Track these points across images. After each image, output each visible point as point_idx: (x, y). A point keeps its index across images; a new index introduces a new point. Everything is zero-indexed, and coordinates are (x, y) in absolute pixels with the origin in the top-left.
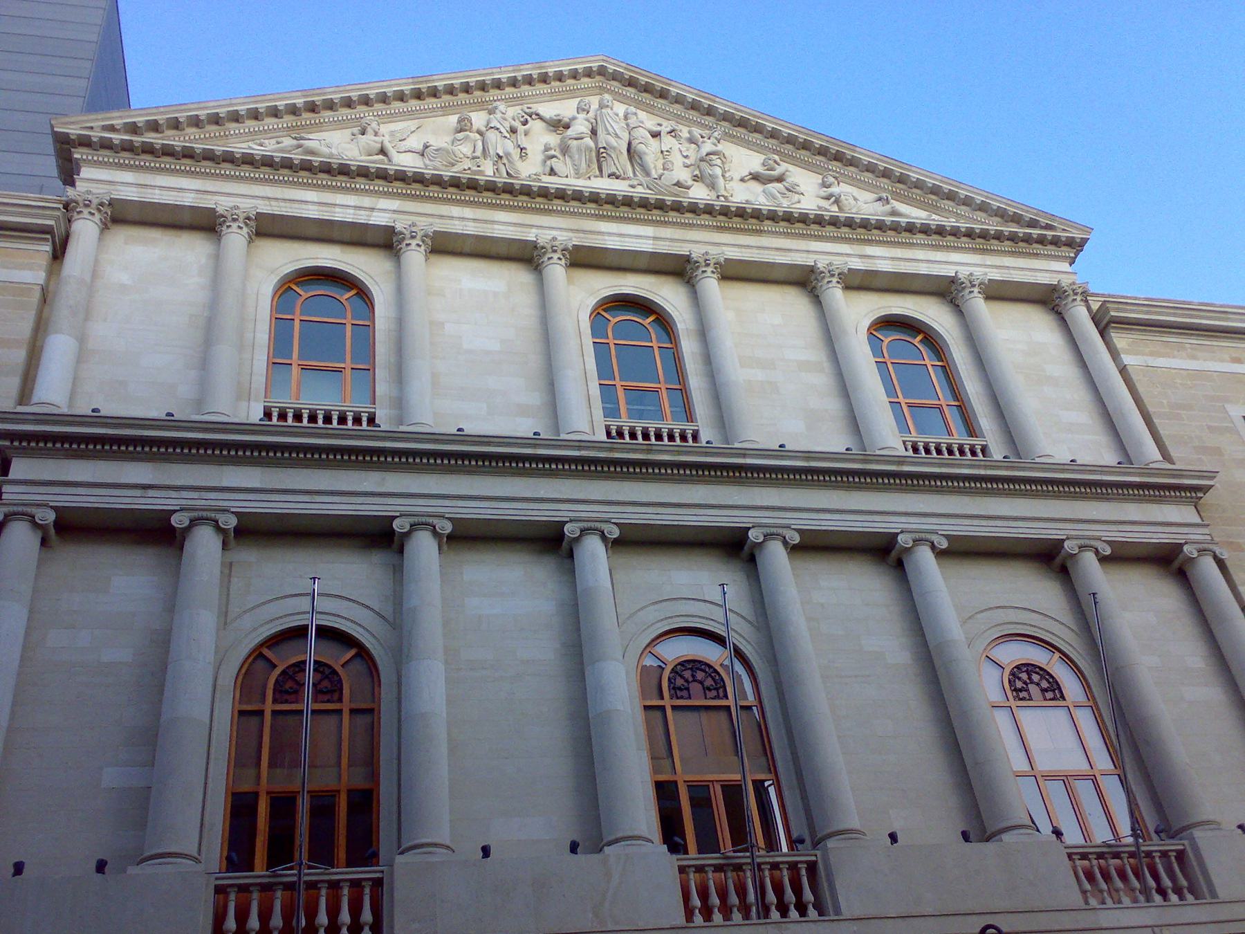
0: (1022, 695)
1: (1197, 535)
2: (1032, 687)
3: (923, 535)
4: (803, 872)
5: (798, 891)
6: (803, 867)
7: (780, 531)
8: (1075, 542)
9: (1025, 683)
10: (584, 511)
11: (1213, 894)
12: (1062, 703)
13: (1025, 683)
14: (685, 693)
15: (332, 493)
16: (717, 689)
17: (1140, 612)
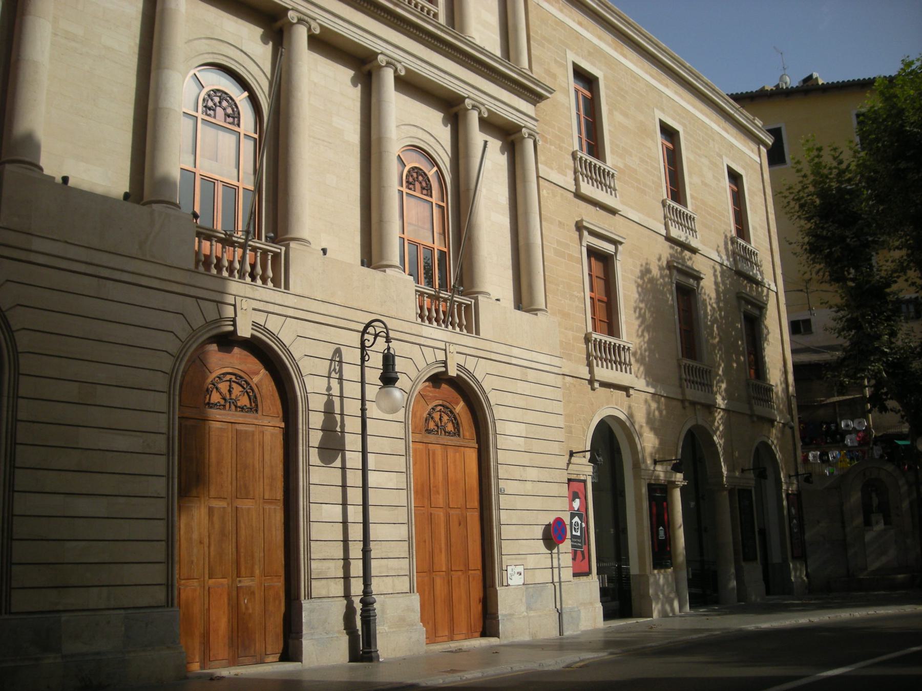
0: (411, 186)
1: (530, 124)
2: (219, 110)
3: (306, 18)
4: (270, 257)
5: (264, 268)
6: (270, 254)
7: (309, 20)
8: (386, 58)
9: (215, 104)
10: (390, 51)
11: (478, 333)
12: (236, 129)
13: (215, 104)
14: (212, 112)
15: (445, 72)
16: (234, 118)
17: (491, 162)
